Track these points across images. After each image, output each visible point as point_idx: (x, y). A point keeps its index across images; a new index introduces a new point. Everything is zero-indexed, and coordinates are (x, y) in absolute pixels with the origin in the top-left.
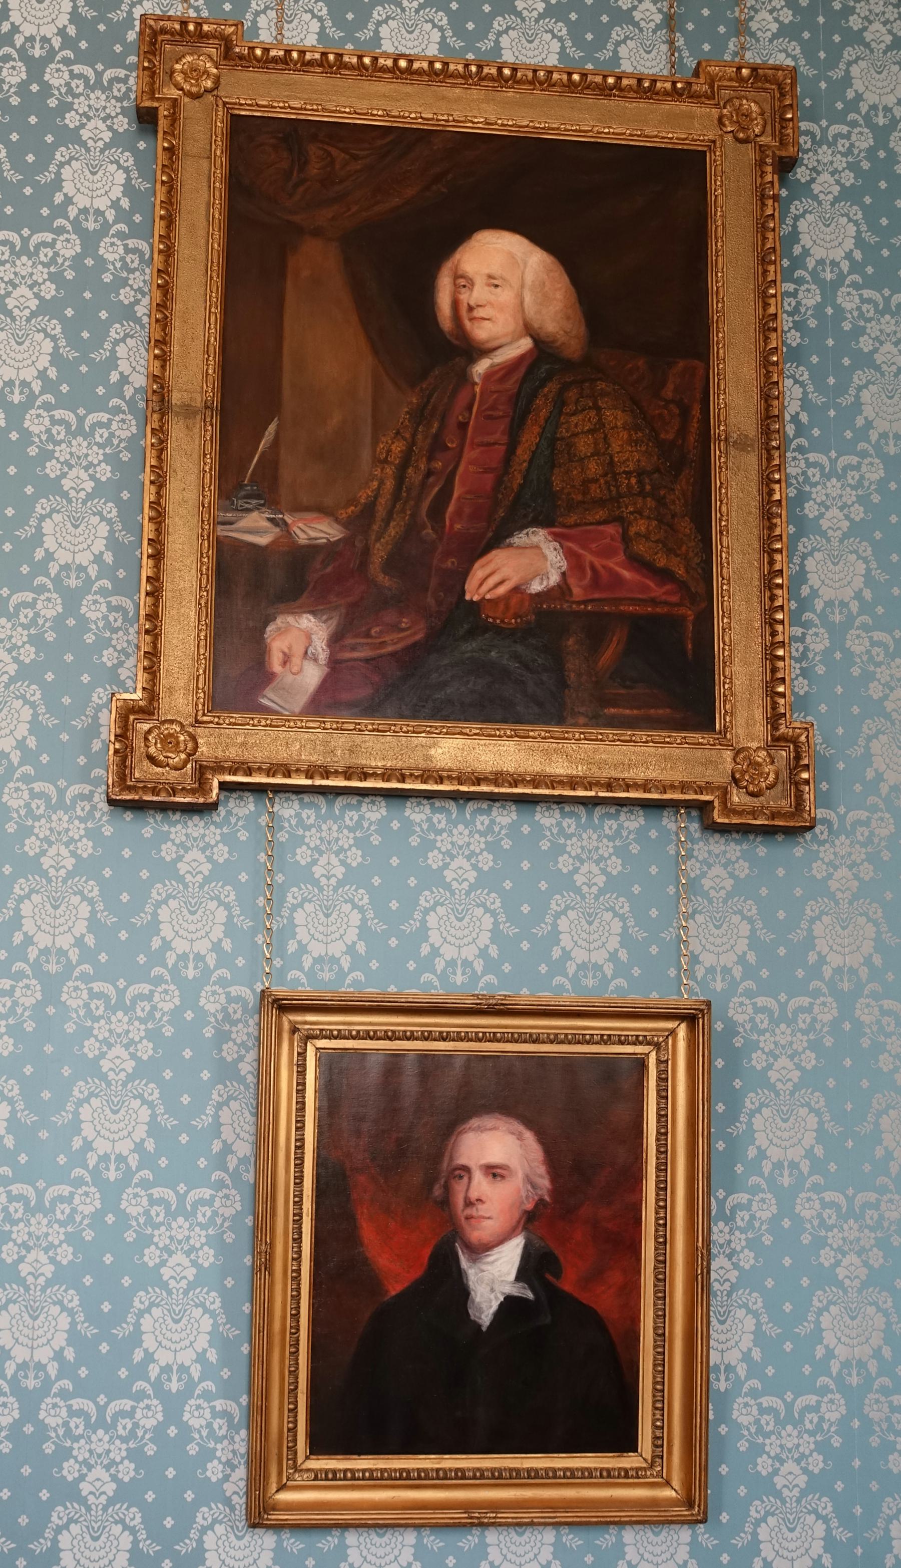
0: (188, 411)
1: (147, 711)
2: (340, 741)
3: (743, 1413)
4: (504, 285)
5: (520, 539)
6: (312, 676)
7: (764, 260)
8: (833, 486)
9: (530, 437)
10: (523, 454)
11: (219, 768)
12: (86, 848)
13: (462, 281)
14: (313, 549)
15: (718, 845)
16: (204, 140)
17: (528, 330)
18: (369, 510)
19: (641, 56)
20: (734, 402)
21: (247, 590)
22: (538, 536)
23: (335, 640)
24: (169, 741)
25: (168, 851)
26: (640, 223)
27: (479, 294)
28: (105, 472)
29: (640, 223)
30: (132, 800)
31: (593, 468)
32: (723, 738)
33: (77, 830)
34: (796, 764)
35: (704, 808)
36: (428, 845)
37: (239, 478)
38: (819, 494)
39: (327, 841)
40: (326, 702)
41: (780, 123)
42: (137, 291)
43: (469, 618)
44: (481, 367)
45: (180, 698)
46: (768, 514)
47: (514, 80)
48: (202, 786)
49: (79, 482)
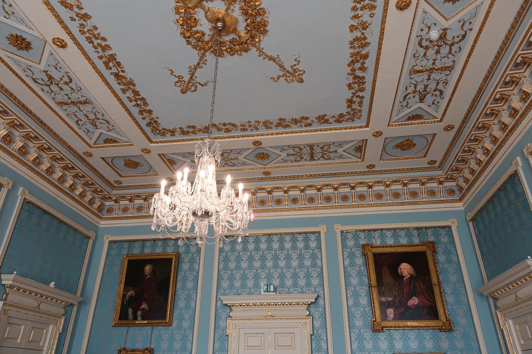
0: (374, 287)
1: (375, 321)
2: (397, 323)
3: (179, 292)
4: (405, 269)
5: (413, 298)
6: (392, 316)
7: (435, 263)
8: (448, 288)
9: (412, 286)
10: (411, 288)
11: (384, 327)
12: (370, 336)
13: (401, 269)
14: (390, 301)
15: (442, 333)
16: (370, 256)
17: (409, 274)
18: (395, 296)
19: (416, 241)
20: (434, 280)
21: (384, 306)
22: (415, 298)
23: (394, 312)
24: (378, 324)
25: (379, 336)
26: (419, 260)
27: (403, 270)
28: (365, 293)
29: (419, 260)
30: (375, 330)
31: (419, 289)
32: (440, 320)
33: (369, 334)
34: (450, 323)
35: (440, 329)
36: (408, 335)
37: (381, 294)
38: (446, 289)
39: (397, 335)
40: (394, 319)
41: (433, 247)
42: (365, 272)
43: (408, 308)
44: (405, 279)
45: (378, 320)
46: (441, 293)
47: (403, 246)
48: (383, 330)
49: (363, 295)
